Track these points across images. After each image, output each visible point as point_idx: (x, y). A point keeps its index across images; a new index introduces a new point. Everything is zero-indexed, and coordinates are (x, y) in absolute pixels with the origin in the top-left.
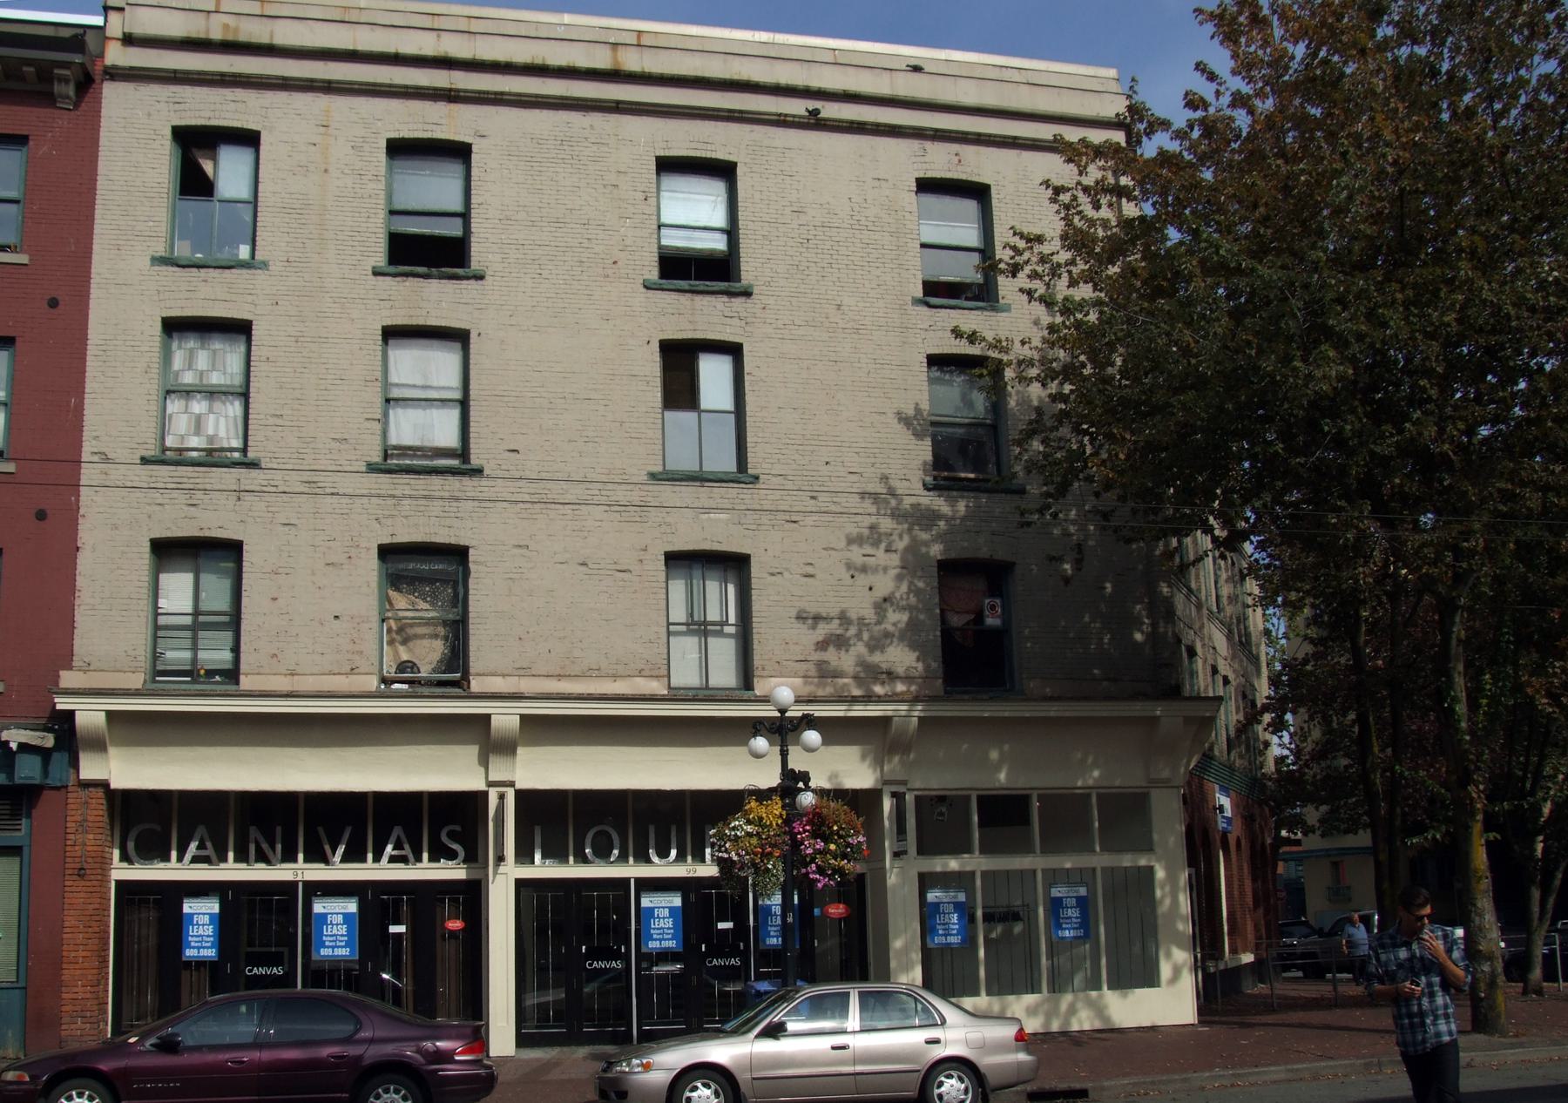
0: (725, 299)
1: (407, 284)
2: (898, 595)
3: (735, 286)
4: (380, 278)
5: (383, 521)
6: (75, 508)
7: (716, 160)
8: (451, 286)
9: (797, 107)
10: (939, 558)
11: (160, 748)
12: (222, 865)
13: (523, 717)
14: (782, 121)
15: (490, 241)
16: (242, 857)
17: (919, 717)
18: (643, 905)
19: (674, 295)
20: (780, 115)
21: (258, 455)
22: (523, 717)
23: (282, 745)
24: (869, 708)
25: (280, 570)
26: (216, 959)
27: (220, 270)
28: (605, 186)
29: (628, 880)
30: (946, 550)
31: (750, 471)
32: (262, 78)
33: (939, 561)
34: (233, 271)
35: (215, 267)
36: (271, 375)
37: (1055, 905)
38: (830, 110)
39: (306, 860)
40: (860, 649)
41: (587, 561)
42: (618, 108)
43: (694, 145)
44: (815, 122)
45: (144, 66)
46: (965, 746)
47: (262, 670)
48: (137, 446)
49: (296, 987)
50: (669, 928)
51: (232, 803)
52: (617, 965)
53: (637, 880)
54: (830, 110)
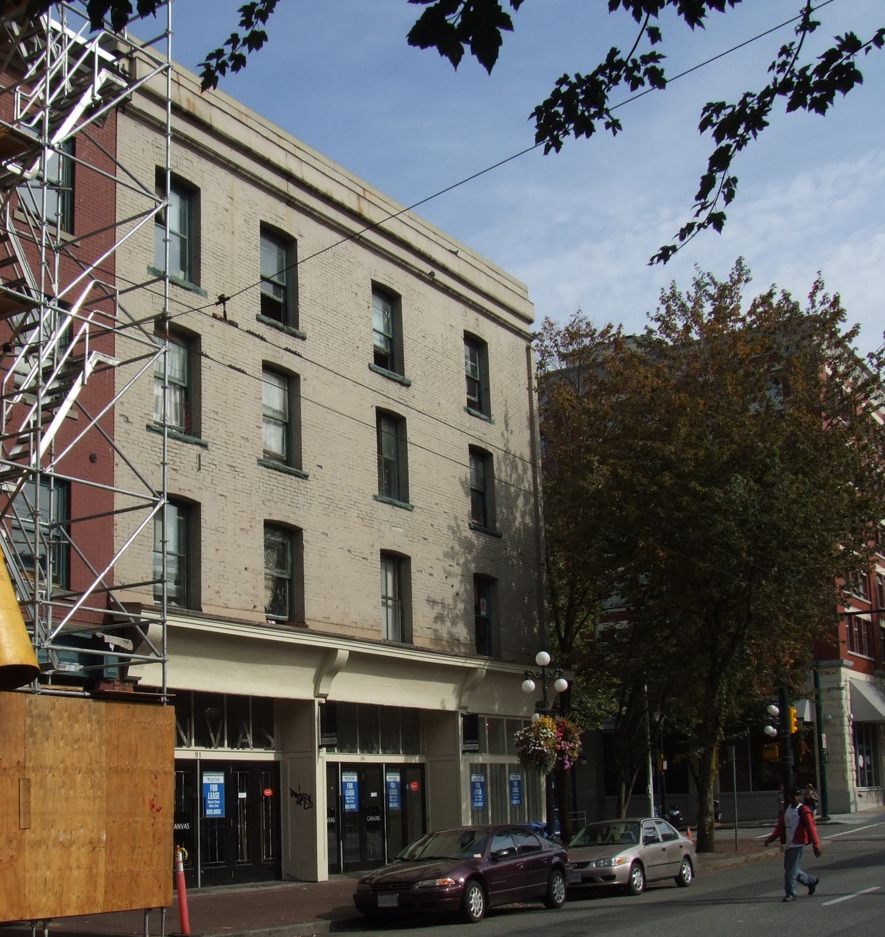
0: (399, 386)
1: (272, 332)
2: (460, 592)
3: (294, 330)
4: (260, 324)
5: (266, 502)
6: (111, 457)
7: (392, 289)
8: (290, 340)
9: (426, 268)
10: (474, 572)
11: (219, 661)
12: (219, 749)
13: (351, 653)
14: (419, 275)
15: (307, 314)
16: (232, 745)
17: (487, 670)
18: (204, 782)
19: (380, 378)
20: (420, 271)
21: (208, 439)
22: (351, 653)
23: (409, 679)
24: (468, 661)
25: (220, 529)
26: (357, 811)
27: (183, 290)
28: (352, 292)
29: (382, 764)
30: (476, 568)
31: (410, 503)
32: (205, 148)
33: (474, 574)
34: (190, 293)
35: (182, 287)
36: (213, 380)
37: (511, 783)
38: (440, 276)
39: (196, 745)
40: (448, 624)
41: (351, 549)
42: (457, 297)
43: (274, 217)
44: (431, 281)
45: (385, 248)
46: (488, 688)
47: (212, 603)
48: (144, 416)
49: (488, 822)
50: (217, 800)
51: (250, 702)
52: (378, 818)
53: (386, 764)
54: (440, 276)
